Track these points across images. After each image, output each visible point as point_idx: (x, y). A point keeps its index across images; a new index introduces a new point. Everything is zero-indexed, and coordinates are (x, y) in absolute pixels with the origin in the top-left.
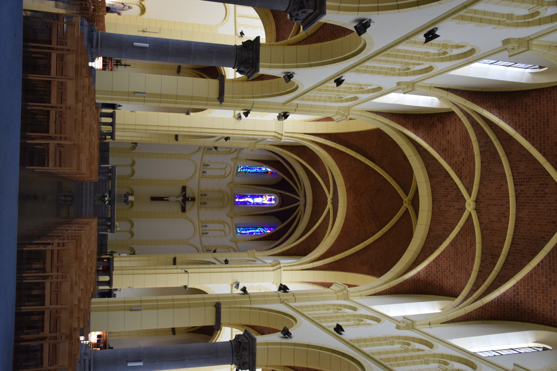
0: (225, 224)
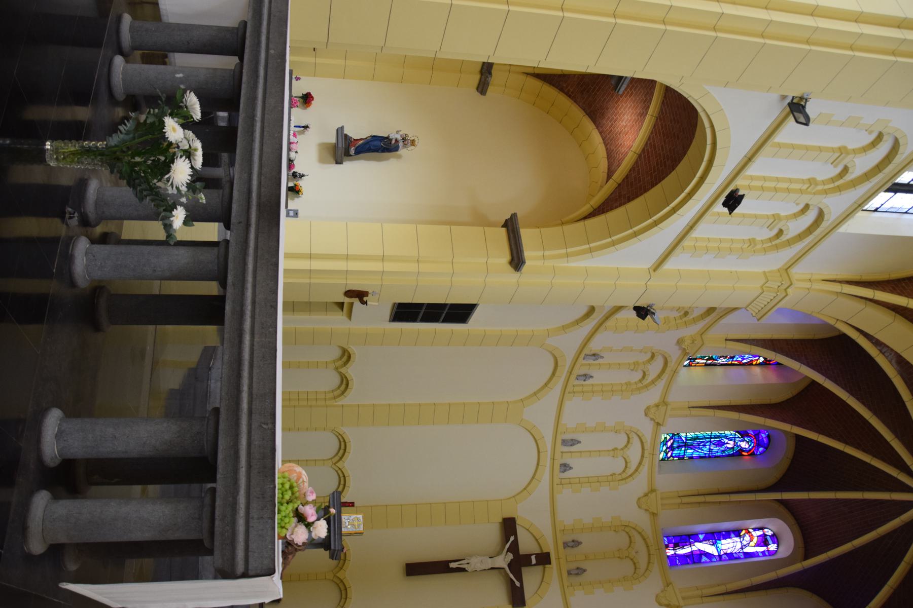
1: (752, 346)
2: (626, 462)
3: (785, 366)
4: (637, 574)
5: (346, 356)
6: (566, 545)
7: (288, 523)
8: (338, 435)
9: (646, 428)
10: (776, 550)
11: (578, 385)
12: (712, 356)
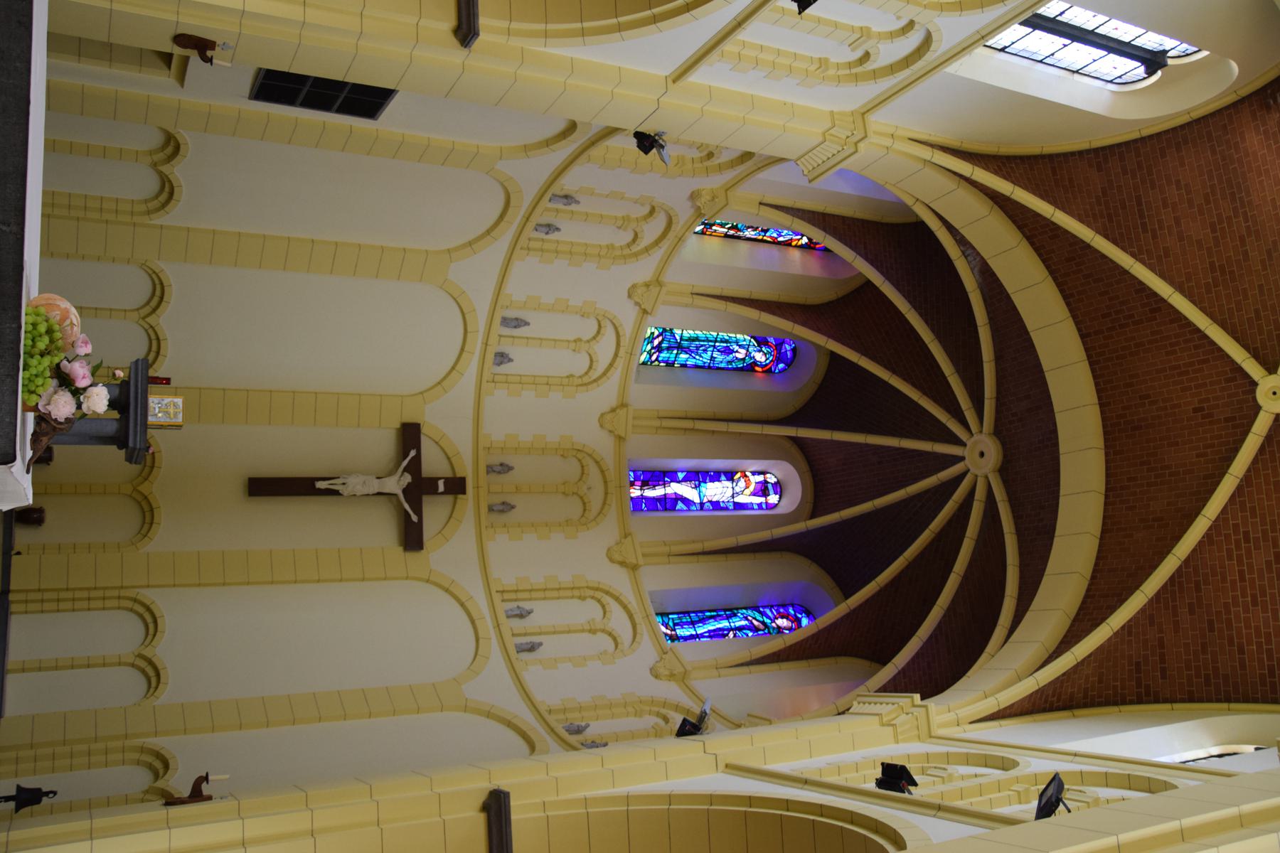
0: (607, 599)
1: (795, 218)
2: (591, 360)
3: (836, 254)
4: (586, 518)
5: (172, 146)
6: (490, 469)
7: (42, 385)
8: (151, 272)
9: (627, 315)
10: (777, 502)
11: (537, 240)
12: (737, 225)
